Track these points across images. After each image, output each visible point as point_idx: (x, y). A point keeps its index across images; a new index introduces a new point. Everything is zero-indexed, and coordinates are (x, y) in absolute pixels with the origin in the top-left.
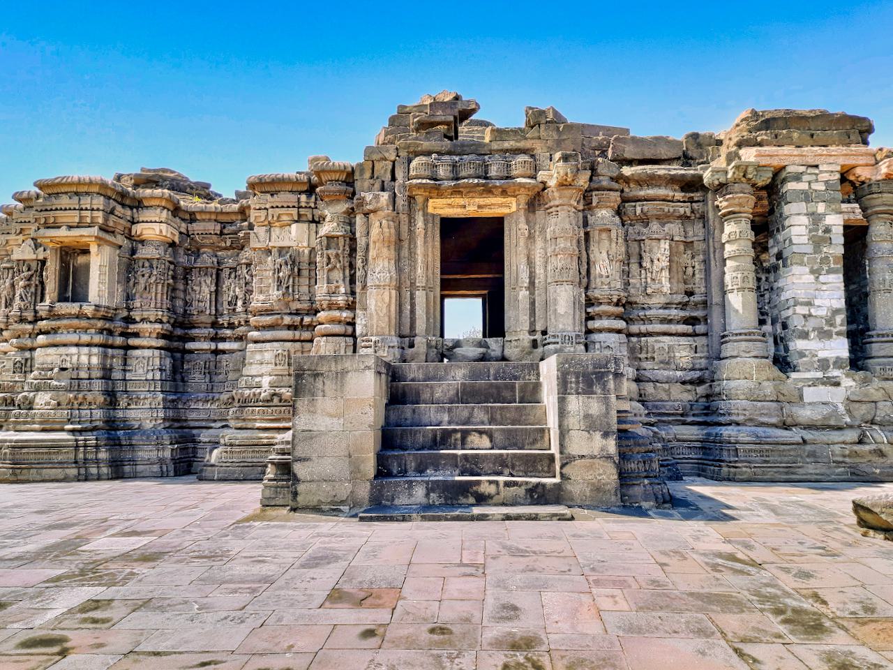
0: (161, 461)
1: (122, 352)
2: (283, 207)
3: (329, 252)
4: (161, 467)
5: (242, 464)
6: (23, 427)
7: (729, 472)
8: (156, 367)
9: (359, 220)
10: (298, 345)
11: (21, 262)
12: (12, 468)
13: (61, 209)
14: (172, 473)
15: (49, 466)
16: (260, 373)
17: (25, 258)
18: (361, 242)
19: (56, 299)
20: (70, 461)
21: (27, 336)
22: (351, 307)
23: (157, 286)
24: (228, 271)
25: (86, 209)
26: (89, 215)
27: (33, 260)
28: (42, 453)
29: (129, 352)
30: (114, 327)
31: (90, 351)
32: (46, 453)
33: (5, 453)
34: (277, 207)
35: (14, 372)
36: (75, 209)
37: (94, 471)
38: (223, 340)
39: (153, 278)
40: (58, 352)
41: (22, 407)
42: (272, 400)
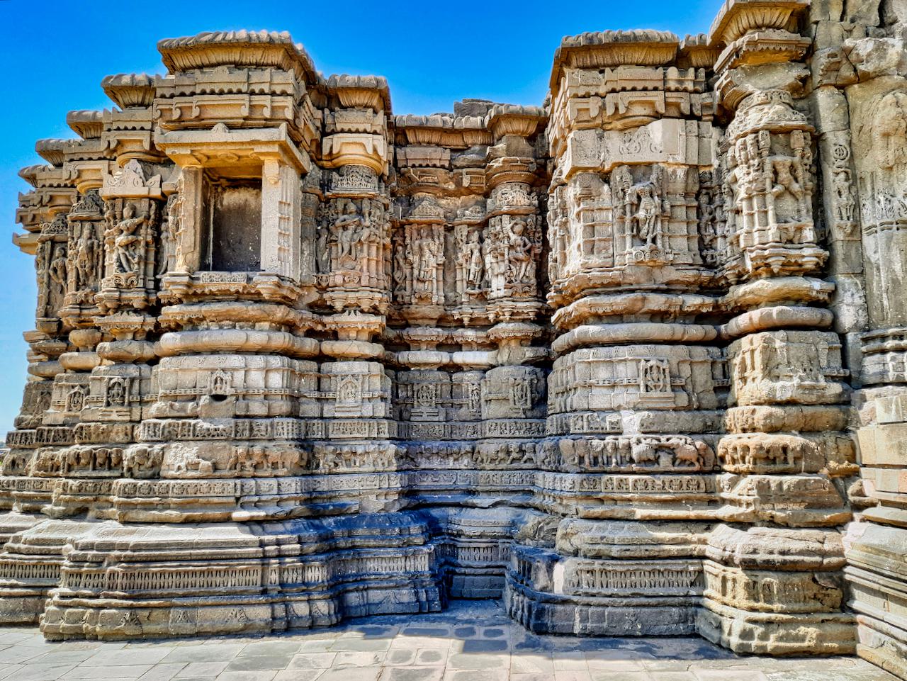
0: (414, 580)
1: (314, 365)
2: (634, 89)
3: (779, 159)
4: (416, 593)
5: (635, 601)
6: (143, 516)
7: (98, 428)
8: (377, 394)
9: (825, 100)
10: (681, 349)
11: (119, 203)
12: (130, 607)
13: (213, 93)
14: (437, 605)
15: (210, 601)
16: (614, 405)
17: (127, 193)
18: (835, 139)
19: (197, 264)
20: (252, 589)
21: (130, 336)
22: (824, 270)
23: (369, 247)
24: (465, 230)
25: (262, 93)
26: (268, 103)
27: (142, 197)
28: (194, 573)
29: (326, 366)
30: (302, 319)
31: (267, 362)
32: (202, 572)
33: (112, 574)
34: (624, 89)
35: (108, 404)
36: (240, 92)
37: (301, 609)
38: (458, 347)
39: (365, 233)
40: (205, 365)
41: (137, 473)
42: (657, 461)
